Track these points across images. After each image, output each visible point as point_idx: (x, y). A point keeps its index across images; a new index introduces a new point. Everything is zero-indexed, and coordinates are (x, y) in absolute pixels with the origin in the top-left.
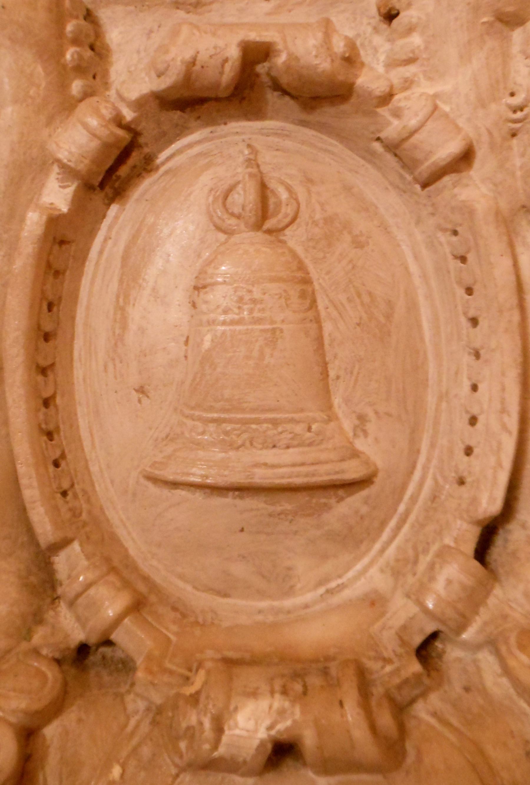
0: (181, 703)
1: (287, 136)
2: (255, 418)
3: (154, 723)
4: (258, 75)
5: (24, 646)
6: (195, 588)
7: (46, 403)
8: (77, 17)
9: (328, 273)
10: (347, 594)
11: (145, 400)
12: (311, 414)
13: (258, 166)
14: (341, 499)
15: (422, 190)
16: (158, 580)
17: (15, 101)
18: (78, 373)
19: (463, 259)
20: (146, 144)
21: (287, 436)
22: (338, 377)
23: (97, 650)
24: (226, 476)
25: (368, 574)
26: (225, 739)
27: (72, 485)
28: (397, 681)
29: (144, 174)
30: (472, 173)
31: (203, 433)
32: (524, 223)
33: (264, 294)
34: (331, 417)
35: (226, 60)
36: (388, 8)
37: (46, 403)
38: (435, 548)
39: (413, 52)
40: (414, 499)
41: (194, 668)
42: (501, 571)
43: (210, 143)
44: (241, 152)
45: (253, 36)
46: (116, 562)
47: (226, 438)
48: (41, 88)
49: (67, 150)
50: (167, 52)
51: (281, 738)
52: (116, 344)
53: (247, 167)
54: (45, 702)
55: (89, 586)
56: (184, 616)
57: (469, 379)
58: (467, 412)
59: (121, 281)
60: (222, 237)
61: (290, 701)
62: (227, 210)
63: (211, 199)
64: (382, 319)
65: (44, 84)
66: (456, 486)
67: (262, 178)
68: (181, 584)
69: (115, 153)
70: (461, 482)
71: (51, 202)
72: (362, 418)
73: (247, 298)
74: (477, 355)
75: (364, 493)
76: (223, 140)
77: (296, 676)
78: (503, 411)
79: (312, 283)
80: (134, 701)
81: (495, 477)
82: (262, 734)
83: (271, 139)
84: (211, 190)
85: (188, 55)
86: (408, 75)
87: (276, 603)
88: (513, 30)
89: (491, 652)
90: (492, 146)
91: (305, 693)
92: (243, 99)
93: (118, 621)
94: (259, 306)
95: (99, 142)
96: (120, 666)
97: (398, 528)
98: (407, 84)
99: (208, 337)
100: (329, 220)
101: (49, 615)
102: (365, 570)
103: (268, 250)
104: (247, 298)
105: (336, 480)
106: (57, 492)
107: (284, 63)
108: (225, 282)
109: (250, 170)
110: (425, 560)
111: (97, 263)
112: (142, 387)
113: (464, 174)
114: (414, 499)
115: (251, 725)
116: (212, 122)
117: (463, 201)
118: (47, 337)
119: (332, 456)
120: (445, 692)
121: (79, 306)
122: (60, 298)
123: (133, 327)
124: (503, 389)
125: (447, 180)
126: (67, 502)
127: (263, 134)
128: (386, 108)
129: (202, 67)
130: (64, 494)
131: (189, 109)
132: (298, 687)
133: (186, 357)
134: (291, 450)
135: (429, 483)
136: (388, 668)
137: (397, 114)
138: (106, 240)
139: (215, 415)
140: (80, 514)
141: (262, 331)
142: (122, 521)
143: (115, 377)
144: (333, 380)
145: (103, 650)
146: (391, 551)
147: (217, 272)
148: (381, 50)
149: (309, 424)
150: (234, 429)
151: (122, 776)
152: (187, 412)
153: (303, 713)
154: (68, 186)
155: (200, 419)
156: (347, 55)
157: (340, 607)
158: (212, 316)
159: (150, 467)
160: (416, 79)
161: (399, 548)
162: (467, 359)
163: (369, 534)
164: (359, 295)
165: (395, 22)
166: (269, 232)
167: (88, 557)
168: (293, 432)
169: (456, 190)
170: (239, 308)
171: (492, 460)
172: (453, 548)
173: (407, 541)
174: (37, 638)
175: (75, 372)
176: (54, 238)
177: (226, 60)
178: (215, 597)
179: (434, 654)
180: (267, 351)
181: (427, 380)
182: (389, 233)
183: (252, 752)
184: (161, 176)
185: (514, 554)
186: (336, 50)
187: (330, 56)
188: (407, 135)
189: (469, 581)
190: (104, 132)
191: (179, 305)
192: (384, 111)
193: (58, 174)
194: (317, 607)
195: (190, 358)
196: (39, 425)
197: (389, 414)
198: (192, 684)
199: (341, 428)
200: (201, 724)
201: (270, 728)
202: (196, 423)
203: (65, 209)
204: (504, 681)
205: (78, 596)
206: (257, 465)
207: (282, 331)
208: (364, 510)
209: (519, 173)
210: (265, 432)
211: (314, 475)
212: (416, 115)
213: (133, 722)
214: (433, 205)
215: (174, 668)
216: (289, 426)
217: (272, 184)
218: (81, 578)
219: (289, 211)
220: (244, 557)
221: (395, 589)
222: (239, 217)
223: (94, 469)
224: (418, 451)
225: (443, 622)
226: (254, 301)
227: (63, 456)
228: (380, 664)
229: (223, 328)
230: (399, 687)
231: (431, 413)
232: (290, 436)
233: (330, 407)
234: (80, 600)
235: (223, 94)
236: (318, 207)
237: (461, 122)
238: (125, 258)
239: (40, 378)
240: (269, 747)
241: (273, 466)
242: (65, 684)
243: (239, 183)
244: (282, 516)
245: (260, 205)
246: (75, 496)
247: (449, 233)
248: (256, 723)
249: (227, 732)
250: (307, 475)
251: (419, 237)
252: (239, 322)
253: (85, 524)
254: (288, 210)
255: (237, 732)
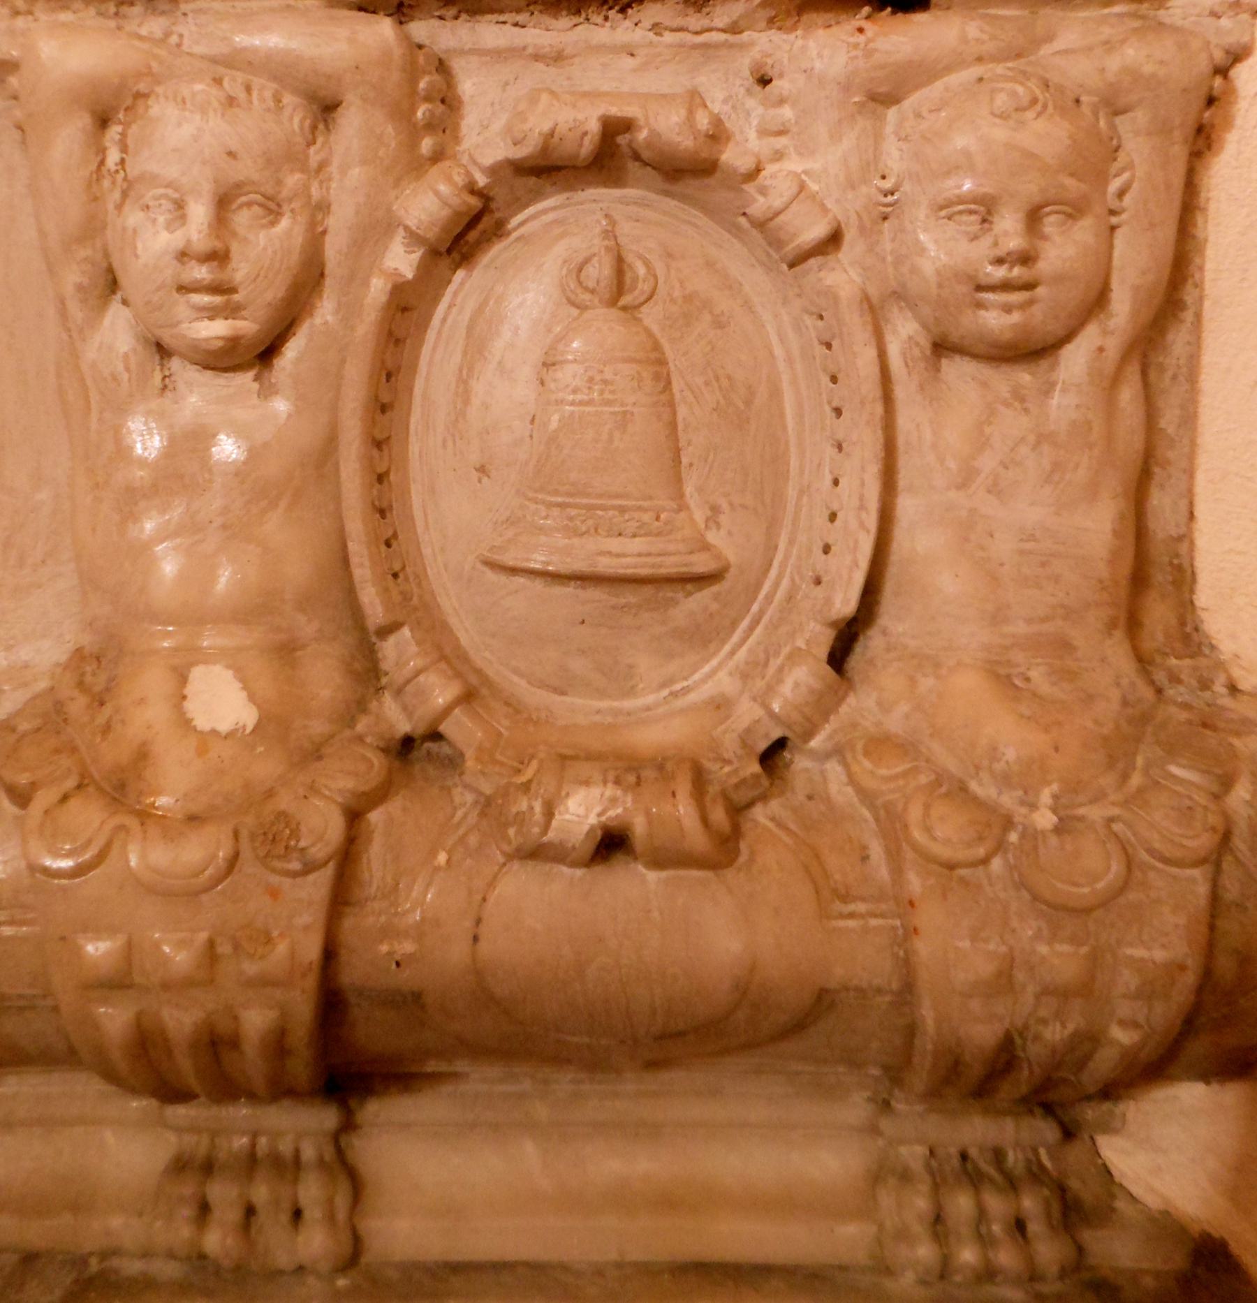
0: (512, 790)
1: (648, 205)
2: (602, 504)
3: (483, 814)
4: (618, 146)
5: (348, 733)
6: (529, 683)
7: (381, 478)
8: (430, 73)
9: (685, 354)
10: (692, 697)
11: (485, 480)
12: (660, 503)
13: (615, 238)
14: (690, 594)
15: (789, 270)
16: (490, 672)
17: (364, 162)
18: (414, 448)
19: (829, 346)
20: (498, 209)
21: (635, 524)
22: (691, 465)
23: (422, 743)
24: (567, 563)
25: (716, 678)
26: (554, 823)
27: (404, 568)
28: (734, 780)
29: (494, 239)
30: (841, 255)
31: (546, 518)
32: (895, 310)
33: (616, 375)
34: (682, 507)
35: (585, 133)
36: (760, 74)
37: (381, 478)
38: (786, 651)
39: (783, 124)
40: (769, 599)
41: (526, 762)
42: (856, 678)
43: (565, 210)
44: (598, 222)
45: (614, 111)
46: (448, 651)
47: (570, 524)
48: (391, 148)
49: (416, 217)
50: (525, 120)
51: (612, 824)
52: (457, 420)
53: (604, 239)
54: (374, 784)
55: (418, 673)
56: (518, 712)
57: (831, 472)
58: (828, 508)
59: (465, 353)
60: (575, 312)
61: (622, 790)
62: (580, 283)
63: (564, 271)
64: (742, 407)
65: (393, 144)
66: (813, 586)
67: (618, 251)
68: (516, 679)
69: (465, 220)
70: (818, 582)
71: (394, 267)
72: (715, 509)
73: (598, 378)
74: (840, 447)
75: (715, 588)
76: (580, 207)
77: (629, 769)
78: (862, 507)
79: (668, 363)
80: (462, 794)
81: (850, 578)
82: (593, 820)
83: (631, 208)
84: (565, 262)
85: (546, 127)
86: (778, 146)
87: (616, 704)
88: (888, 108)
89: (839, 762)
90: (862, 229)
91: (638, 784)
92: (603, 167)
93: (447, 711)
94: (610, 387)
95: (450, 211)
96: (447, 762)
97: (751, 629)
98: (777, 156)
99: (556, 417)
100: (688, 299)
101: (374, 705)
102: (714, 672)
103: (622, 328)
104: (598, 378)
105: (683, 573)
106: (388, 574)
107: (645, 139)
108: (575, 361)
109: (606, 242)
110: (775, 664)
111: (439, 332)
112: (483, 466)
113: (829, 257)
114: (769, 599)
115: (581, 811)
116: (570, 188)
117: (829, 286)
118: (384, 408)
119: (681, 547)
120: (787, 799)
121: (417, 376)
122: (399, 368)
123: (476, 402)
124: (863, 484)
125: (812, 262)
126: (399, 585)
127: (622, 203)
128: (752, 184)
129: (561, 139)
130: (395, 576)
131: (545, 175)
132: (631, 778)
133: (531, 436)
134: (637, 539)
135: (785, 583)
136: (727, 769)
137: (763, 191)
138: (450, 307)
139: (560, 499)
140: (411, 599)
141: (612, 413)
142: (455, 609)
143: (455, 455)
144: (685, 468)
145: (428, 745)
146: (742, 654)
147: (567, 349)
148: (753, 115)
149: (658, 512)
150: (579, 515)
151: (448, 861)
152: (531, 494)
153: (634, 801)
154: (415, 252)
155: (543, 502)
156: (711, 133)
157: (682, 711)
158: (561, 395)
159: (489, 551)
160: (787, 151)
161: (750, 651)
162: (831, 451)
163: (718, 634)
164: (717, 379)
165: (768, 87)
166: (624, 308)
167: (418, 643)
168: (641, 521)
169: (822, 274)
170: (589, 388)
171: (848, 560)
172: (804, 650)
173: (759, 643)
174: (360, 727)
175: (410, 447)
176: (398, 306)
177: (585, 133)
178: (551, 694)
179: (781, 764)
180: (617, 435)
181: (788, 471)
182: (753, 312)
183: (582, 837)
184: (512, 243)
185: (871, 662)
186: (699, 127)
187: (693, 133)
188: (771, 215)
189: (817, 685)
190: (455, 201)
191: (527, 382)
192: (750, 188)
193: (404, 238)
194: (661, 710)
195: (535, 439)
196: (373, 504)
197: (744, 507)
198: (524, 775)
199: (692, 520)
200: (531, 808)
201: (599, 815)
202: (539, 506)
203: (410, 275)
204: (849, 790)
205: (408, 681)
206: (602, 553)
207: (632, 414)
208: (714, 606)
209: (889, 259)
210: (610, 519)
211: (660, 566)
212: (781, 196)
213: (459, 814)
214: (800, 286)
215: (505, 760)
216: (636, 515)
217: (629, 258)
218: (412, 663)
219: (645, 288)
220: (583, 652)
221: (742, 693)
222: (593, 292)
223: (427, 551)
224: (776, 548)
225: (789, 727)
226: (605, 382)
227: (395, 535)
228: (718, 766)
229: (572, 408)
230: (737, 786)
231: (790, 508)
232: (638, 524)
233: (680, 495)
234: (409, 688)
235: (579, 163)
236: (677, 285)
237: (829, 204)
238: (470, 329)
239: (375, 452)
240: (599, 833)
241: (618, 556)
242: (390, 772)
243: (595, 255)
244: (625, 609)
245: (615, 282)
246: (407, 579)
247: (815, 317)
248: (587, 809)
249: (557, 817)
250: (653, 566)
251: (786, 318)
252: (590, 402)
253: (416, 609)
254: (644, 287)
255: (567, 817)
